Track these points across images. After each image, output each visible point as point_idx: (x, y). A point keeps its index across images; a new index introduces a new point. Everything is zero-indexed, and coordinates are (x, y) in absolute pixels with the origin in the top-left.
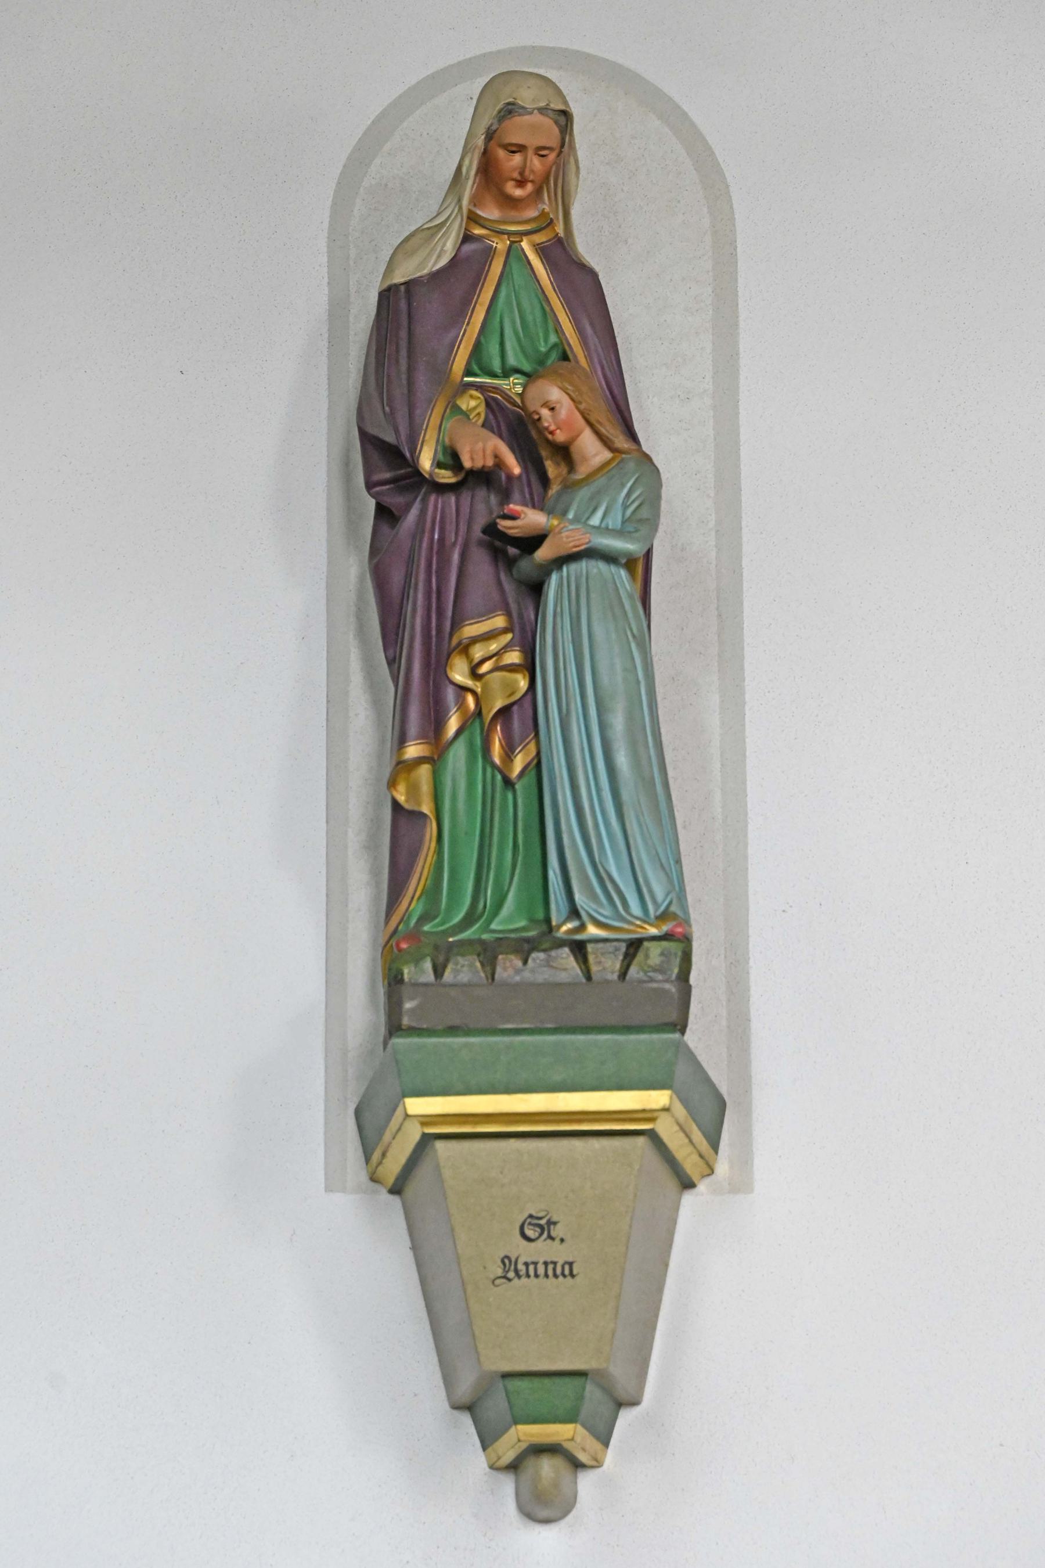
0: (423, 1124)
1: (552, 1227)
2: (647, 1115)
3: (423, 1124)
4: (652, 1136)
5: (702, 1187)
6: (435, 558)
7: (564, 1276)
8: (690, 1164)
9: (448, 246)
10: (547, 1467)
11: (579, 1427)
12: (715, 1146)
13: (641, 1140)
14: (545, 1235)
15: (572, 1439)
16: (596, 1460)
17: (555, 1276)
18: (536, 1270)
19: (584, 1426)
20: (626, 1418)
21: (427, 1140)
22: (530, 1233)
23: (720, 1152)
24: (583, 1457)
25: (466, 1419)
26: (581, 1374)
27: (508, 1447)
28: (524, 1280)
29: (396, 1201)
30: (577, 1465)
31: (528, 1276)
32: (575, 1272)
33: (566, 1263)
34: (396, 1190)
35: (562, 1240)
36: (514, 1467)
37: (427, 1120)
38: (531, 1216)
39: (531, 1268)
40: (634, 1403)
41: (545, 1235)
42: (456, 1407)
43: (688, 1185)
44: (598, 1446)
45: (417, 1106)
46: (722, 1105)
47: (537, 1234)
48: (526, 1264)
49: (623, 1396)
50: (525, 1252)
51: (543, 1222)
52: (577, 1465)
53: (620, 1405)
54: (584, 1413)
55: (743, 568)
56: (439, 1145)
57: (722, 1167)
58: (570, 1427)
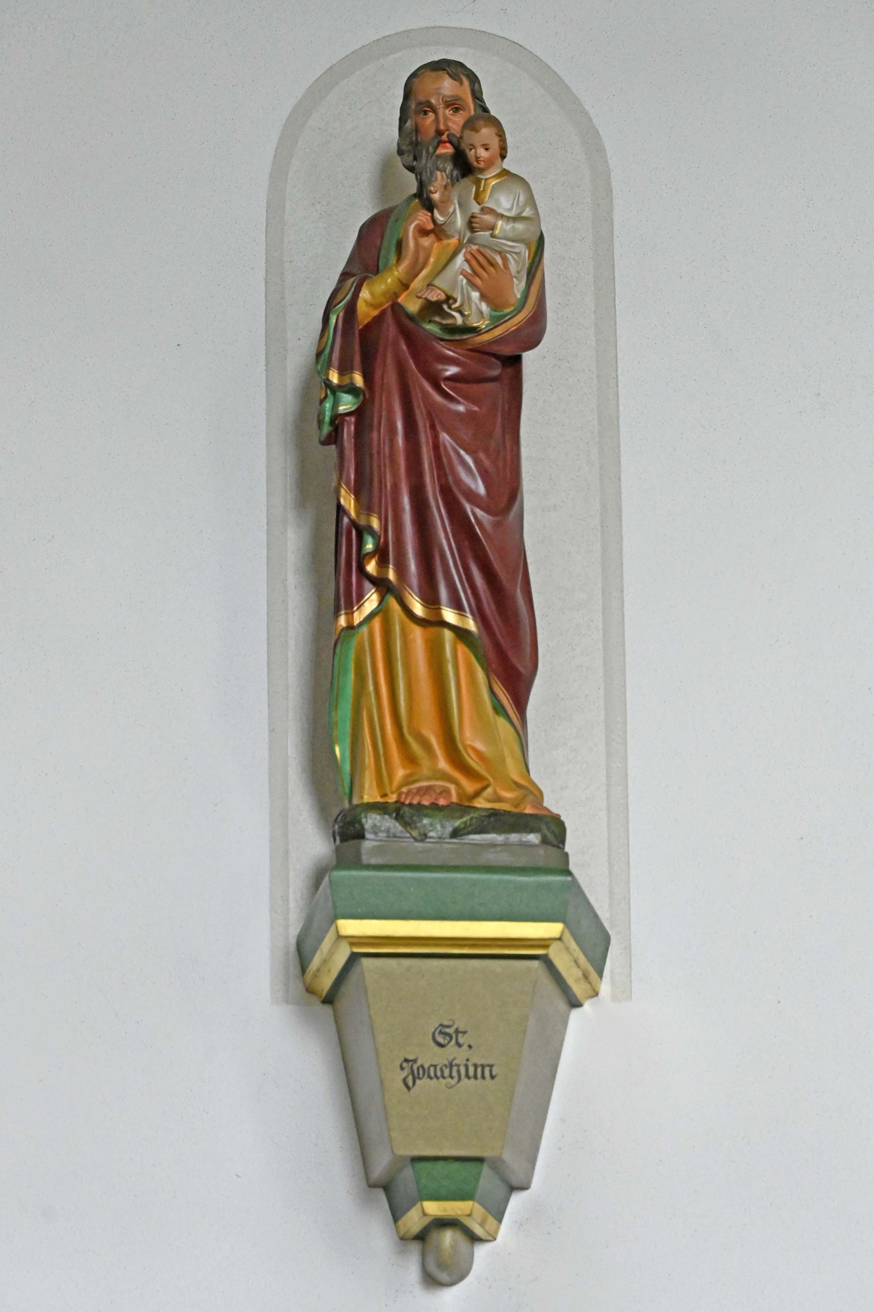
0: (352, 944)
1: (460, 1035)
2: (544, 943)
3: (352, 944)
4: (546, 960)
5: (587, 1006)
6: (388, 470)
7: (437, 1078)
8: (578, 989)
9: (442, 223)
10: (448, 1237)
11: (476, 1204)
12: (600, 974)
13: (535, 964)
14: (453, 1041)
15: (469, 1215)
16: (491, 1235)
17: (467, 1076)
18: (483, 1073)
19: (478, 1202)
20: (516, 1201)
21: (354, 958)
22: (440, 1039)
23: (603, 979)
24: (478, 1231)
25: (381, 1195)
26: (480, 1160)
27: (413, 1221)
28: (480, 1081)
29: (327, 1009)
30: (474, 1239)
31: (475, 1077)
32: (494, 1073)
33: (431, 1065)
34: (329, 1000)
35: (470, 1047)
36: (421, 1237)
37: (355, 941)
38: (441, 1025)
39: (479, 1070)
40: (524, 1188)
41: (453, 1041)
42: (372, 1186)
43: (575, 1004)
44: (491, 1221)
45: (350, 927)
46: (607, 940)
47: (446, 1042)
48: (476, 1066)
49: (515, 1182)
50: (430, 1056)
51: (450, 1031)
52: (474, 1239)
53: (513, 1188)
54: (477, 1196)
55: (266, 413)
56: (365, 962)
57: (605, 988)
58: (469, 1204)
